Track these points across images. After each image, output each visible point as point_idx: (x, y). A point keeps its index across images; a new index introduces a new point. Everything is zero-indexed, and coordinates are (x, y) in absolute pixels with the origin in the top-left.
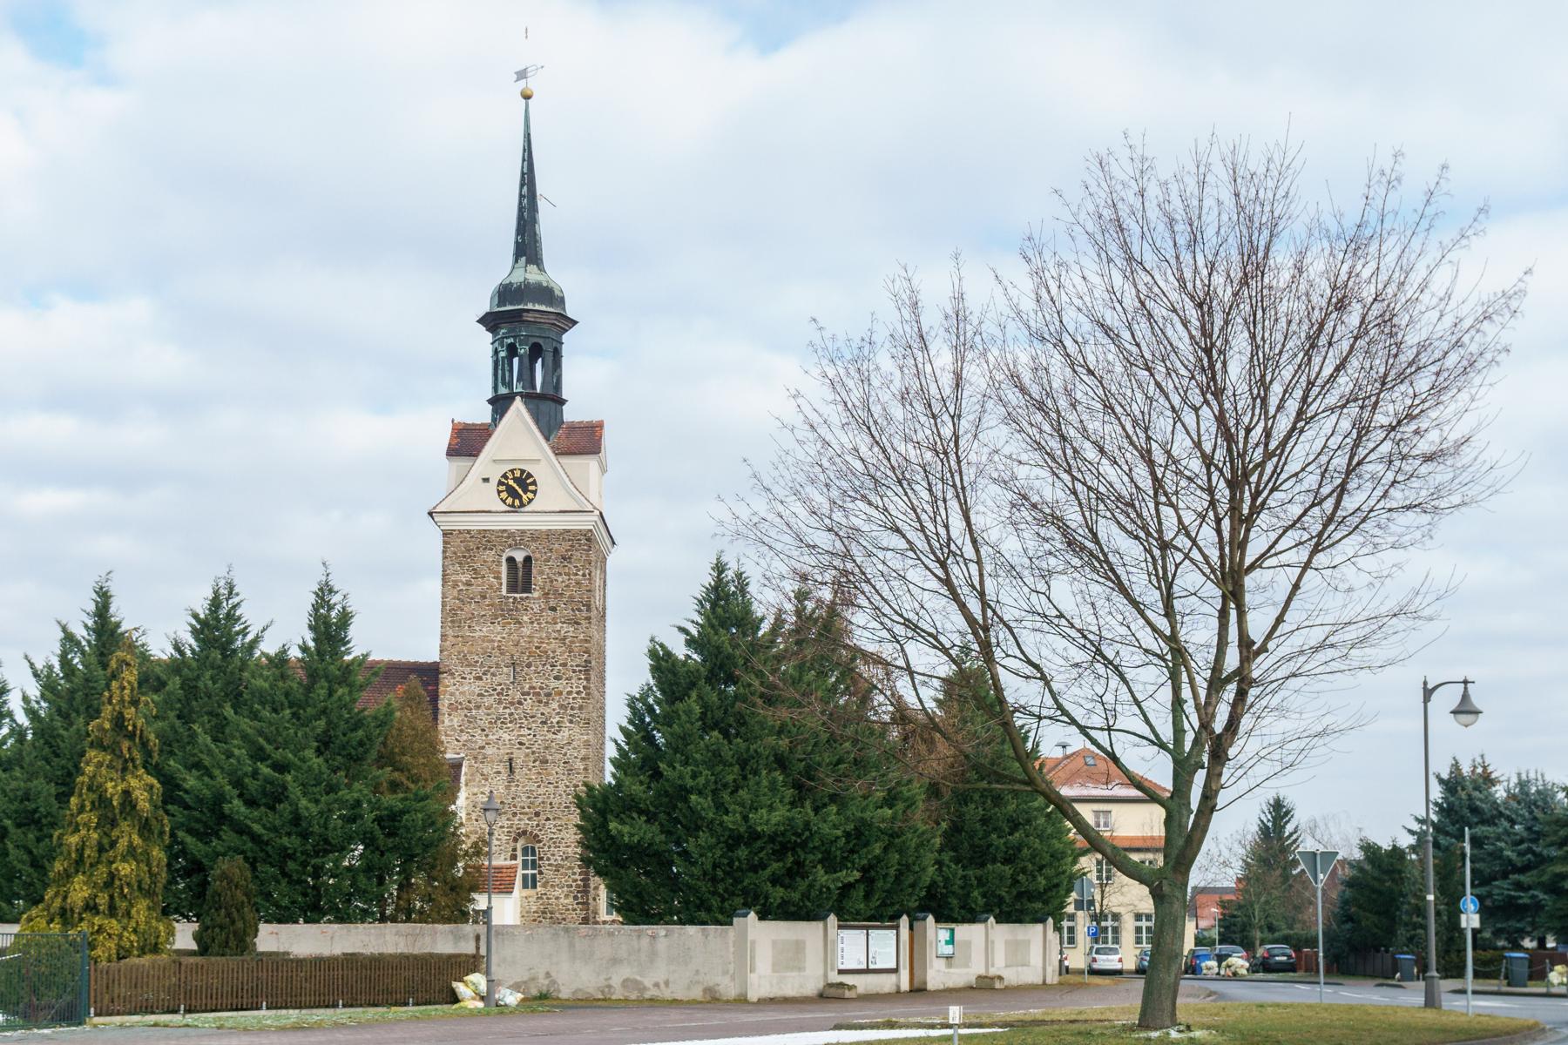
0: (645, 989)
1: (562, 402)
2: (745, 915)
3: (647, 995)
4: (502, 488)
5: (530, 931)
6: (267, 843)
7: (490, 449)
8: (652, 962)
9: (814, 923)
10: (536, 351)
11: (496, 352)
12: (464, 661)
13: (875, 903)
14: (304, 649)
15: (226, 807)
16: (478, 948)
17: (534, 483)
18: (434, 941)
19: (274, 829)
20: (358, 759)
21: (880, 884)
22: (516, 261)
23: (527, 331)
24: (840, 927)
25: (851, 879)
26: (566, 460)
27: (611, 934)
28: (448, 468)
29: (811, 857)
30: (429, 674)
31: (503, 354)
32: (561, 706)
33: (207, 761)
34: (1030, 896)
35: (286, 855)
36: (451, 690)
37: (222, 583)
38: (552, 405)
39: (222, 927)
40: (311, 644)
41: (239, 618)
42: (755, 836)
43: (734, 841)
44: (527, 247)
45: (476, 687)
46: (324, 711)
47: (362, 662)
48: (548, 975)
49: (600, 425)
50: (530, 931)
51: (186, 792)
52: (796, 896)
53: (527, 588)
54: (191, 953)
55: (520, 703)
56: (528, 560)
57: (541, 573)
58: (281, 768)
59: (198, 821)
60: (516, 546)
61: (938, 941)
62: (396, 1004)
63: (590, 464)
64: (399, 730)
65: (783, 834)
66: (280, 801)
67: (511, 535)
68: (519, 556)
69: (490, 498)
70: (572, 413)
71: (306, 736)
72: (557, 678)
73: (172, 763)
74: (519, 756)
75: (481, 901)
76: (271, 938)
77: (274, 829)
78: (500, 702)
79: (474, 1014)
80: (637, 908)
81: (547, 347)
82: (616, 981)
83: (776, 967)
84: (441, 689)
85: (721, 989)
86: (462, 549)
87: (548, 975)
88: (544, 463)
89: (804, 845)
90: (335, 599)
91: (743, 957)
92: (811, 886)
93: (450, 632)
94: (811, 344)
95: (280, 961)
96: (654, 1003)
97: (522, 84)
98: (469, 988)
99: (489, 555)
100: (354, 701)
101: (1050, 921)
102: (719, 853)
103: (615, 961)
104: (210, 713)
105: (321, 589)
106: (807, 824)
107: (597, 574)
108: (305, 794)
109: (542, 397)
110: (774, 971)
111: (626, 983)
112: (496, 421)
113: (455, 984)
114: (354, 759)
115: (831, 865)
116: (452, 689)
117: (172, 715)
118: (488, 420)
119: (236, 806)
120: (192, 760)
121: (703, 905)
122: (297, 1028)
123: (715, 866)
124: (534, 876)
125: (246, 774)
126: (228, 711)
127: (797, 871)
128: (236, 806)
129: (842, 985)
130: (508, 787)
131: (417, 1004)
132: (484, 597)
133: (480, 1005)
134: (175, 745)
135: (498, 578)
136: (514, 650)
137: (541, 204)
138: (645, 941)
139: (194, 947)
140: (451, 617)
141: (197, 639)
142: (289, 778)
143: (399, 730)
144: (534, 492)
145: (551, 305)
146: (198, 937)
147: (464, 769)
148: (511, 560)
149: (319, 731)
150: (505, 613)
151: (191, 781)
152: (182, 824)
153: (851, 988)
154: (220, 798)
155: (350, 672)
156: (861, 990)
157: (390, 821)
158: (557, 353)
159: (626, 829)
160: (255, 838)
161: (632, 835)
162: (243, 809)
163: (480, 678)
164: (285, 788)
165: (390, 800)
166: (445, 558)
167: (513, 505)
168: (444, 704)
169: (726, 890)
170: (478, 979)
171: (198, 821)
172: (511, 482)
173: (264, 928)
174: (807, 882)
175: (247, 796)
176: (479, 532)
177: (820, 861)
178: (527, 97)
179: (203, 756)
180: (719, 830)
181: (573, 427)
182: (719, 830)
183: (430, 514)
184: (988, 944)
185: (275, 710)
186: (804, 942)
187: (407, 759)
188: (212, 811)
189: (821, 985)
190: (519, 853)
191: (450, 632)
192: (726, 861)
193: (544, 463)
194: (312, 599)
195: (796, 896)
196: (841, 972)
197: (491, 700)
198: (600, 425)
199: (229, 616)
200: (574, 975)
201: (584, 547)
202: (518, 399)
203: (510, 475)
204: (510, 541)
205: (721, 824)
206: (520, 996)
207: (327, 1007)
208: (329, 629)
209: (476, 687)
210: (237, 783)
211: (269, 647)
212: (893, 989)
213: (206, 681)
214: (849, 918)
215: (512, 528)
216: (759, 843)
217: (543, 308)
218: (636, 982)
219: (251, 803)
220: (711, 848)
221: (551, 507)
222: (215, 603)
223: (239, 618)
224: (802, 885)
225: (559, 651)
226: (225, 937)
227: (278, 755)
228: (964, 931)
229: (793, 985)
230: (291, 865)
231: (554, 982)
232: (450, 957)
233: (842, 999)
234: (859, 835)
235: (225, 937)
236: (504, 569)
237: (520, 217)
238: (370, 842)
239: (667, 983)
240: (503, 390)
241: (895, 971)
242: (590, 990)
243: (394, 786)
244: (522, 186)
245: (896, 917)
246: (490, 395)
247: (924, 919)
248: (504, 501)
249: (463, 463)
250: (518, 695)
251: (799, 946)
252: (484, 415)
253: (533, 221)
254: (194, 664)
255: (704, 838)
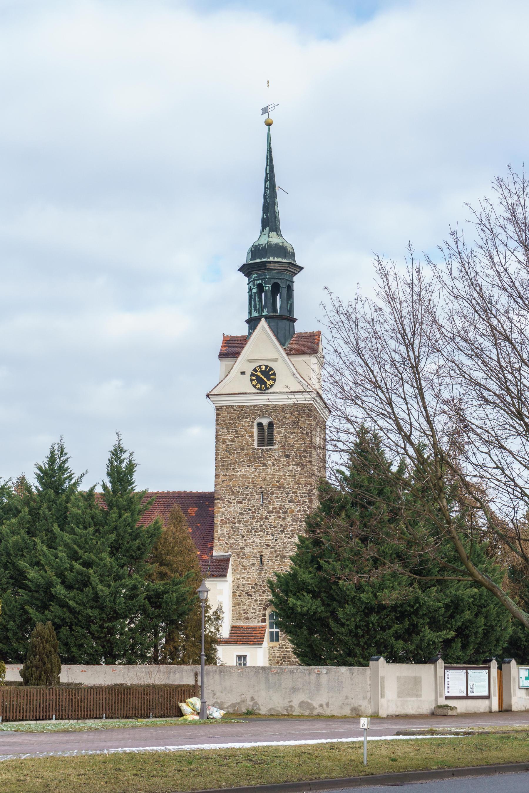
0: (314, 708)
1: (294, 320)
2: (377, 660)
3: (315, 712)
4: (253, 378)
5: (247, 673)
6: (78, 613)
7: (247, 352)
8: (318, 690)
9: (427, 666)
10: (276, 289)
11: (250, 289)
12: (230, 491)
13: (470, 651)
14: (105, 487)
15: (53, 590)
16: (196, 681)
17: (274, 374)
18: (182, 678)
19: (83, 604)
20: (137, 558)
21: (472, 638)
22: (263, 230)
24: (446, 668)
25: (449, 636)
26: (294, 358)
27: (291, 672)
28: (219, 366)
29: (421, 621)
30: (204, 503)
31: (254, 291)
32: (293, 520)
33: (43, 561)
35: (90, 621)
36: (223, 511)
37: (56, 447)
38: (287, 322)
39: (37, 667)
40: (109, 485)
41: (67, 469)
42: (382, 607)
43: (369, 610)
44: (270, 220)
45: (238, 509)
46: (115, 528)
47: (144, 495)
48: (252, 699)
50: (247, 673)
51: (30, 580)
52: (412, 647)
53: (270, 443)
54: (20, 684)
55: (267, 518)
56: (271, 424)
57: (279, 433)
58: (87, 564)
59: (37, 599)
60: (262, 415)
61: (519, 678)
62: (141, 717)
64: (166, 539)
65: (401, 605)
66: (86, 586)
67: (260, 408)
68: (265, 422)
70: (301, 327)
71: (103, 544)
72: (290, 502)
73: (21, 562)
74: (267, 553)
76: (71, 674)
77: (83, 604)
78: (254, 518)
79: (194, 723)
80: (311, 655)
81: (283, 285)
82: (295, 703)
83: (400, 694)
84: (216, 510)
85: (362, 708)
86: (228, 418)
87: (252, 699)
88: (280, 361)
89: (416, 613)
90: (124, 456)
91: (377, 688)
92: (422, 640)
93: (221, 473)
94: (322, 303)
95: (76, 689)
96: (319, 717)
97: (266, 116)
98: (190, 706)
99: (246, 422)
100: (135, 521)
101: (494, 665)
102: (359, 618)
103: (294, 690)
104: (47, 530)
105: (115, 450)
106: (417, 599)
108: (101, 582)
109: (281, 318)
110: (399, 697)
111: (301, 704)
112: (250, 334)
113: (180, 704)
114: (136, 558)
115: (435, 625)
116: (222, 510)
117: (22, 531)
118: (246, 333)
119: (59, 590)
120: (34, 560)
121: (350, 653)
122: (66, 731)
123: (357, 627)
124: (277, 633)
125: (66, 569)
126: (56, 529)
127: (413, 630)
128: (59, 590)
129: (446, 707)
130: (259, 574)
131: (155, 717)
132: (243, 449)
133: (197, 718)
134: (25, 551)
135: (252, 436)
136: (262, 483)
137: (279, 193)
138: (313, 677)
139: (21, 679)
140: (222, 462)
141: (41, 483)
142: (91, 571)
143: (166, 539)
144: (274, 380)
145: (285, 257)
146: (23, 674)
147: (231, 562)
148: (260, 425)
149: (111, 541)
150: (257, 460)
151: (32, 574)
152: (28, 601)
153: (452, 708)
154: (50, 585)
155: (132, 503)
156: (459, 711)
157: (155, 599)
158: (290, 289)
159: (299, 603)
160: (71, 610)
161: (302, 607)
162: (63, 591)
163: (240, 503)
164: (89, 578)
165: (158, 585)
166: (217, 424)
167: (260, 389)
168: (218, 520)
169: (365, 643)
170: (196, 701)
171: (37, 599)
172: (259, 374)
173: (64, 667)
174: (419, 638)
175: (67, 583)
176: (239, 407)
177: (428, 624)
178: (269, 124)
179: (41, 558)
180: (359, 604)
181: (301, 336)
182: (359, 604)
183: (208, 396)
185: (85, 528)
186: (420, 678)
187: (169, 557)
188: (46, 592)
189: (433, 706)
190: (267, 617)
191: (221, 473)
192: (364, 624)
193: (280, 361)
194: (109, 456)
195: (412, 647)
196: (447, 698)
197: (248, 517)
199: (61, 468)
202: (263, 320)
203: (259, 370)
204: (259, 412)
205: (360, 599)
206: (223, 712)
207: (96, 718)
208: (121, 475)
209: (238, 509)
210: (61, 575)
211: (83, 488)
212: (487, 710)
213: (44, 510)
214: (452, 662)
215: (261, 404)
216: (385, 612)
217: (280, 260)
218: (308, 704)
219: (69, 587)
220: (354, 615)
222: (52, 460)
223: (67, 469)
224: (416, 639)
225: (291, 484)
226: (40, 673)
227: (86, 556)
229: (412, 707)
230: (94, 627)
231: (256, 704)
232: (178, 686)
233: (446, 716)
234: (455, 607)
235: (40, 673)
236: (255, 431)
237: (265, 202)
238: (144, 611)
239: (328, 705)
240: (255, 314)
241: (488, 697)
242: (279, 709)
243: (162, 576)
244: (266, 182)
245: (488, 661)
246: (247, 317)
247: (509, 662)
248: (255, 386)
249: (229, 362)
250: (266, 514)
251: (417, 681)
252: (242, 330)
253: (274, 203)
254: (38, 499)
255: (349, 608)
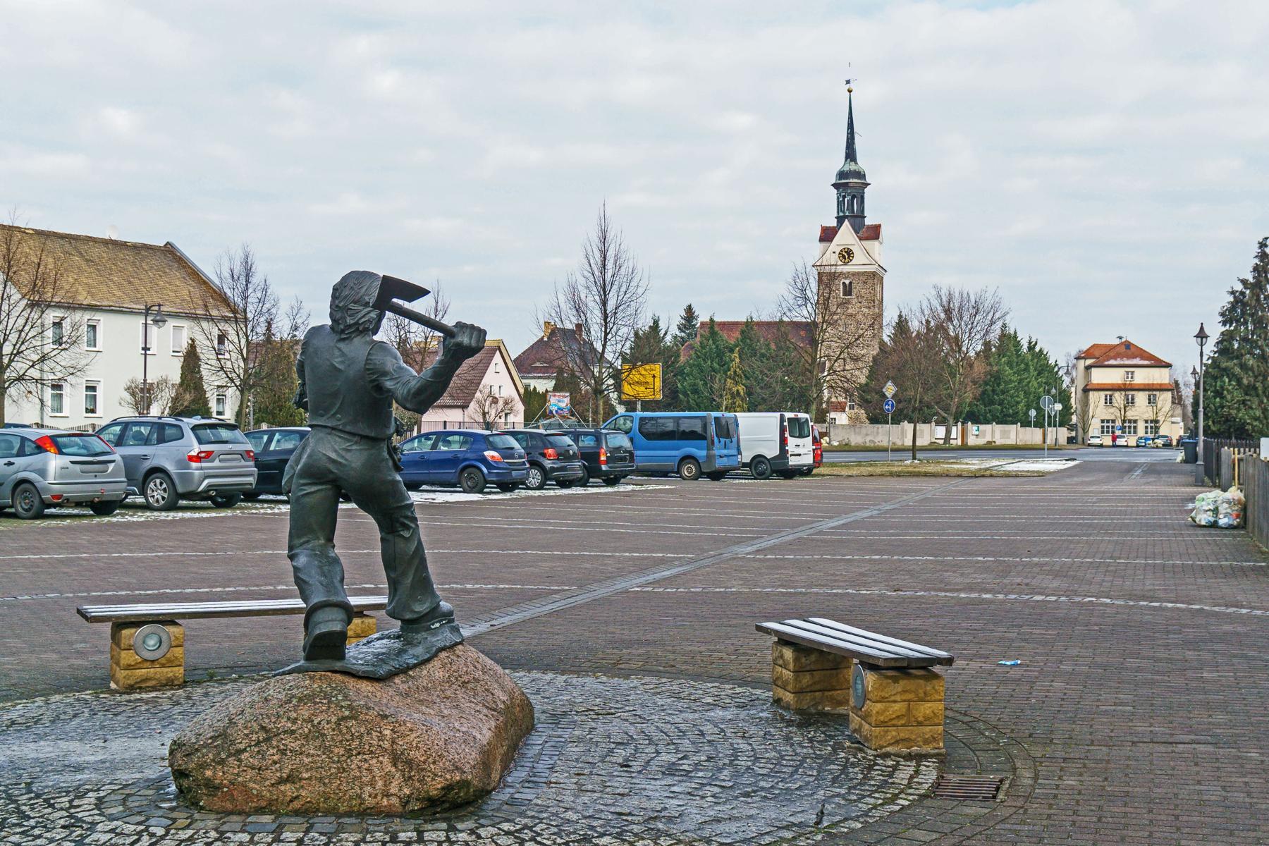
23: (850, 187)
26: (866, 243)
30: (810, 331)
34: (1009, 416)
44: (851, 155)
49: (880, 226)
63: (876, 243)
68: (847, 282)
69: (834, 259)
75: (833, 415)
107: (878, 288)
137: (856, 136)
178: (850, 91)
184: (993, 432)
198: (880, 226)
200: (856, 439)
201: (874, 278)
221: (859, 262)
228: (982, 427)
249: (825, 244)
252: (834, 223)
